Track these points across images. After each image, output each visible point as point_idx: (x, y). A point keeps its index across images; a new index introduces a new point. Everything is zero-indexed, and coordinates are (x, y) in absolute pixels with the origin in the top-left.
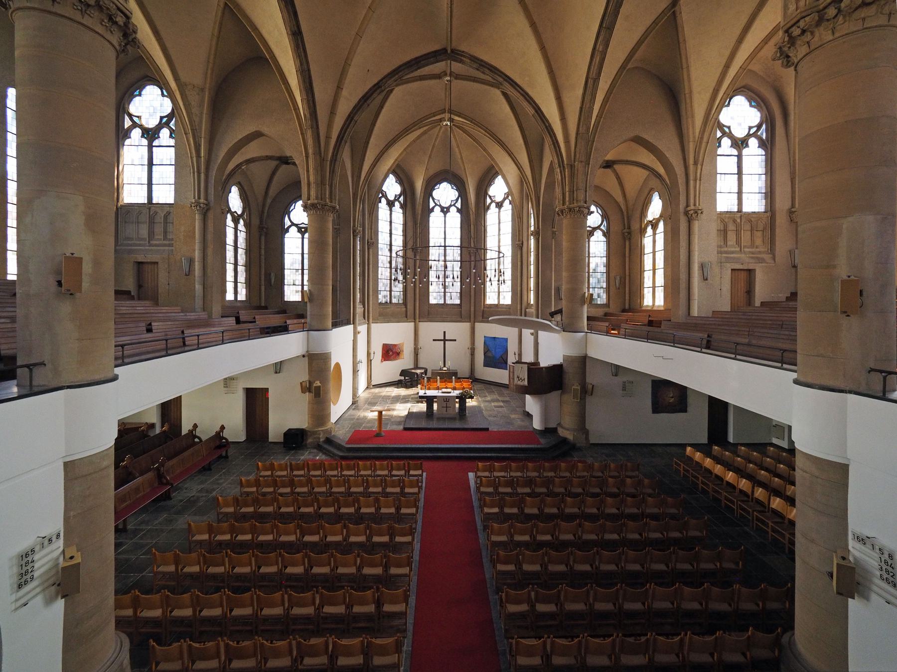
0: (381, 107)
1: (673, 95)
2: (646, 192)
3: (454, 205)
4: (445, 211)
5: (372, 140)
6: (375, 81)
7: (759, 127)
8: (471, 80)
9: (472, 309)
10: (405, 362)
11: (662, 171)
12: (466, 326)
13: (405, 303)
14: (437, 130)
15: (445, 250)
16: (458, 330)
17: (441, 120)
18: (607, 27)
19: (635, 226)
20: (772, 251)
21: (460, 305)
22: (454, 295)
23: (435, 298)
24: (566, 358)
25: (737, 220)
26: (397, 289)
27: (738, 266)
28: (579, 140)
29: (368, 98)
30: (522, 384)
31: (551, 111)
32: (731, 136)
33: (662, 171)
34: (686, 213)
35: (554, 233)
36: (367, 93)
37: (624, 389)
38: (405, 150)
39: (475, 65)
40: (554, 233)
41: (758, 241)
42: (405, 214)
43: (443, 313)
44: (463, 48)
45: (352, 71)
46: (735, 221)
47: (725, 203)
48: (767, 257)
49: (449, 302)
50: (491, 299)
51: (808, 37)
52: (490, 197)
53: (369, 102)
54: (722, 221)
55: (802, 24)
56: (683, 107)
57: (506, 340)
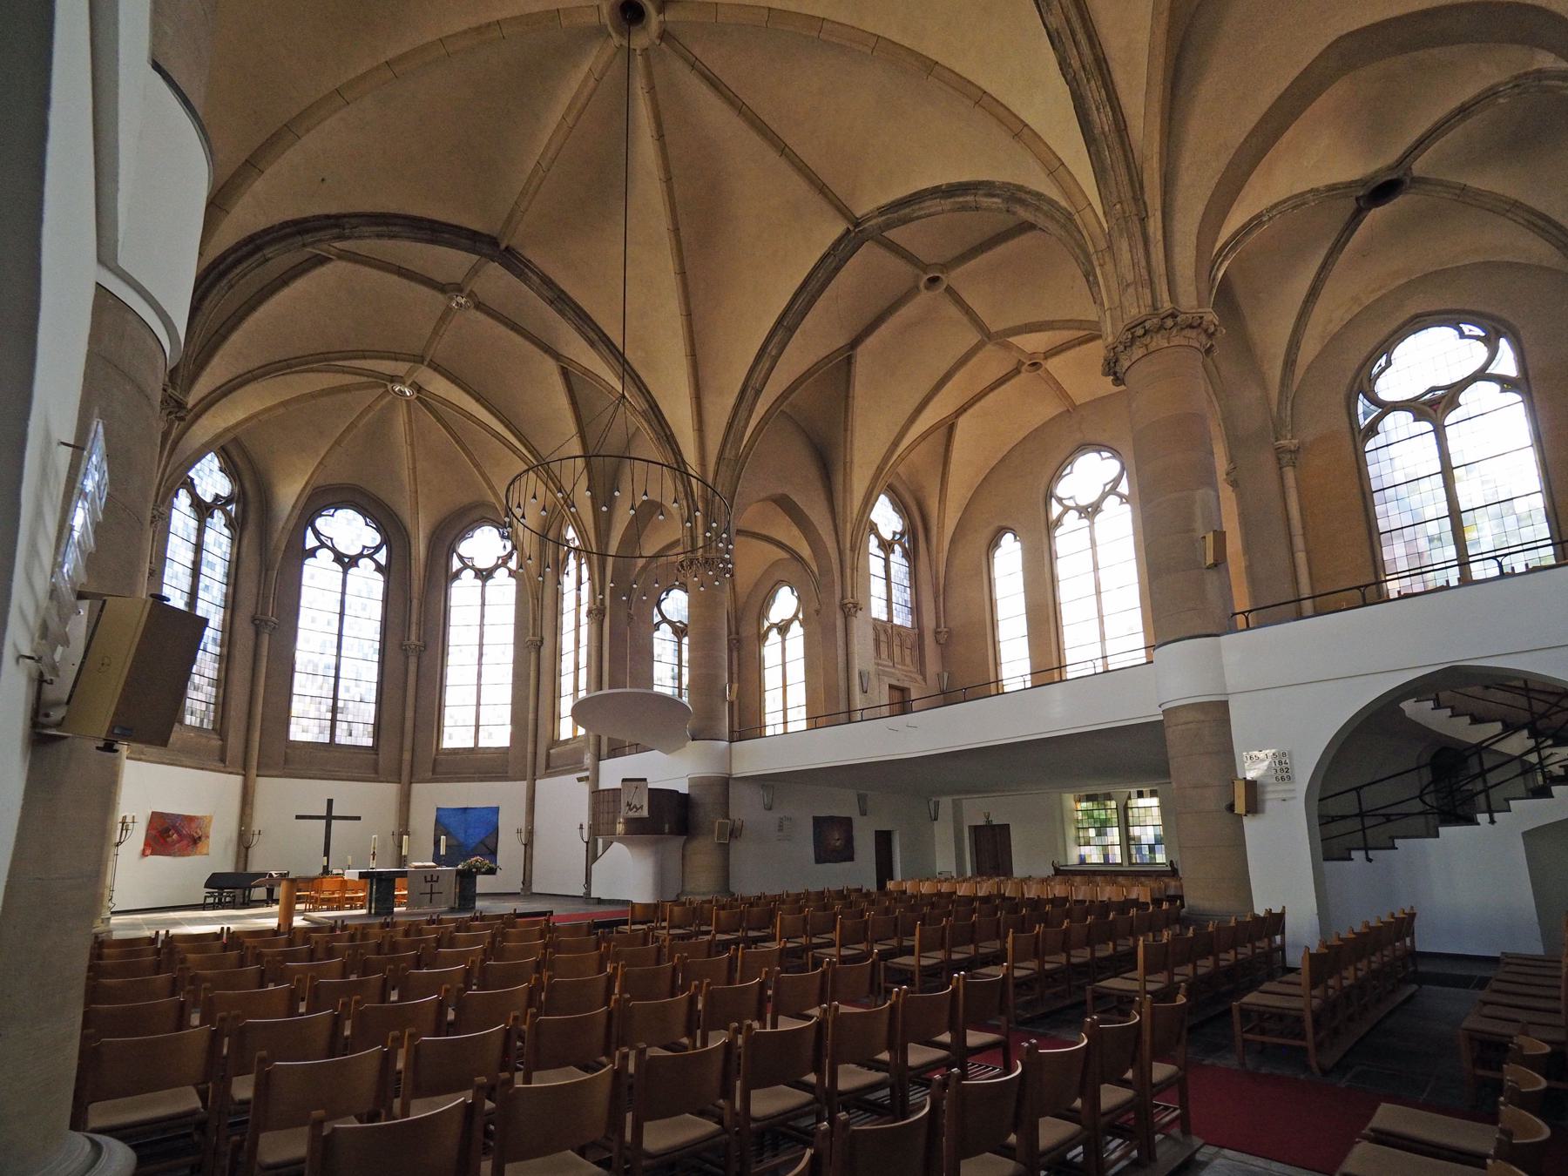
0: (284, 280)
1: (827, 462)
2: (771, 583)
3: (370, 557)
4: (346, 562)
5: (236, 337)
6: (333, 209)
7: (902, 534)
8: (506, 325)
9: (407, 756)
10: (217, 856)
11: (805, 551)
12: (390, 790)
13: (220, 727)
14: (370, 396)
15: (328, 826)
16: (368, 800)
17: (393, 379)
18: (786, 325)
19: (748, 631)
20: (923, 673)
21: (374, 749)
22: (358, 729)
23: (305, 727)
24: (694, 783)
25: (885, 631)
26: (201, 696)
27: (895, 683)
28: (723, 468)
29: (307, 231)
30: (637, 815)
31: (680, 415)
32: (878, 536)
33: (805, 551)
34: (843, 606)
35: (630, 617)
36: (306, 220)
37: (781, 828)
38: (284, 404)
39: (549, 294)
40: (630, 617)
41: (908, 660)
42: (237, 540)
43: (327, 760)
44: (529, 253)
45: (291, 158)
46: (885, 632)
47: (878, 610)
48: (919, 678)
49: (342, 738)
50: (456, 736)
51: (1147, 339)
52: (461, 558)
53: (308, 238)
54: (875, 628)
55: (1148, 325)
56: (839, 479)
57: (495, 811)
